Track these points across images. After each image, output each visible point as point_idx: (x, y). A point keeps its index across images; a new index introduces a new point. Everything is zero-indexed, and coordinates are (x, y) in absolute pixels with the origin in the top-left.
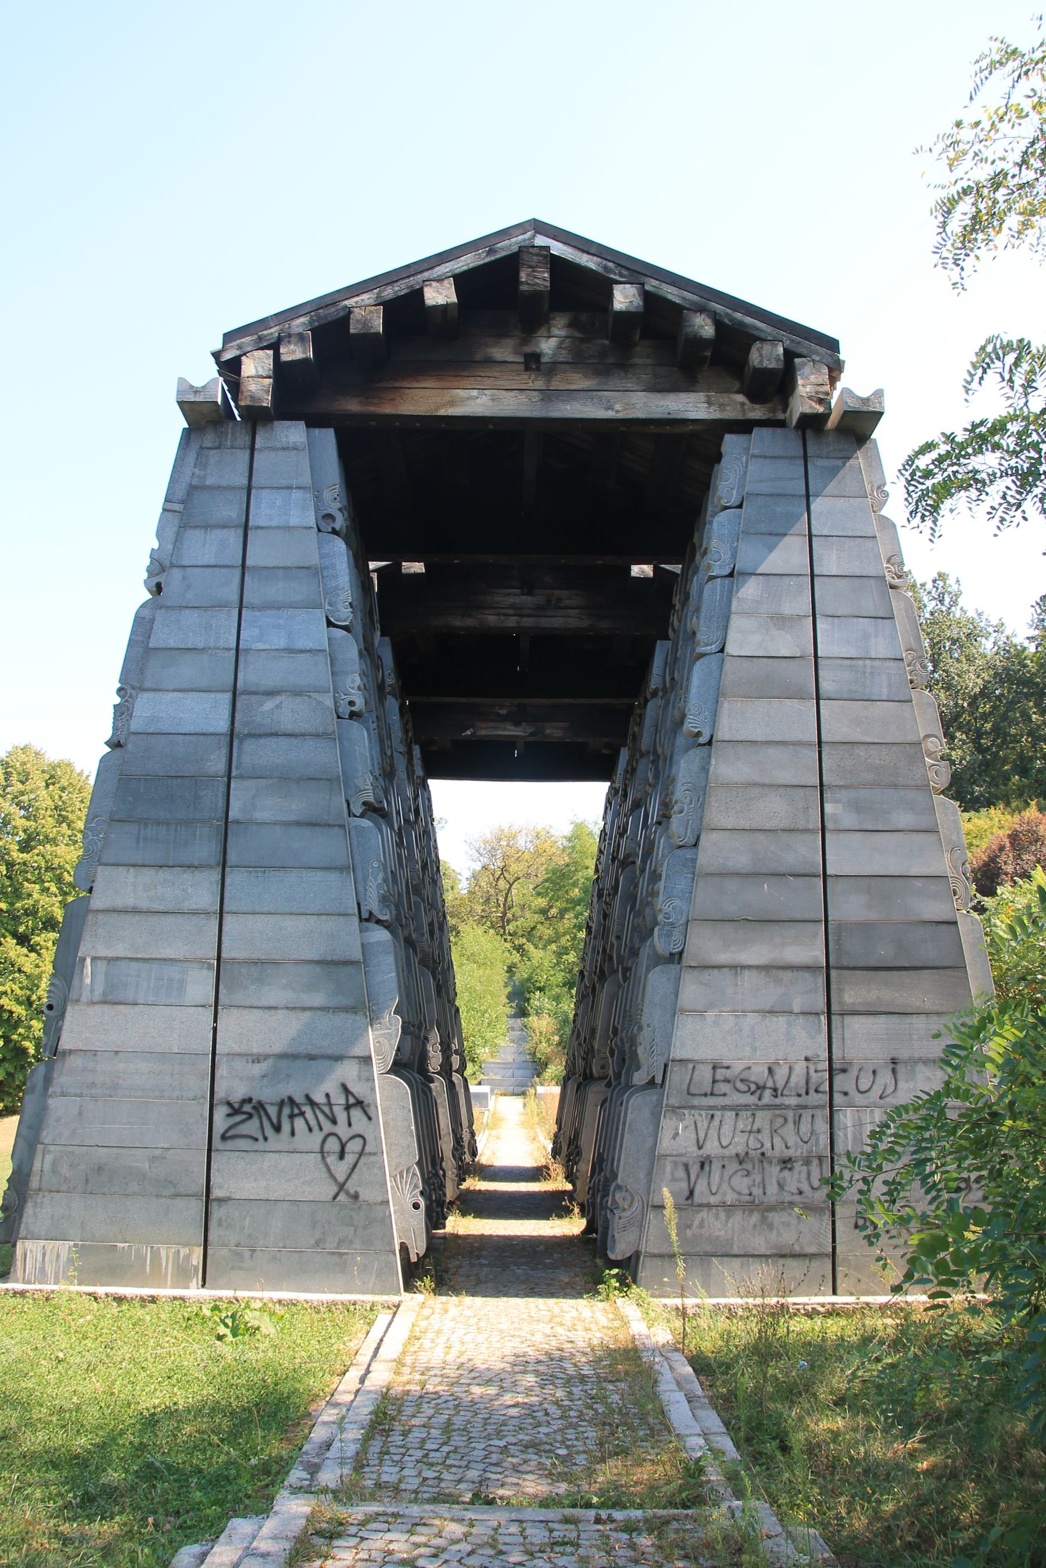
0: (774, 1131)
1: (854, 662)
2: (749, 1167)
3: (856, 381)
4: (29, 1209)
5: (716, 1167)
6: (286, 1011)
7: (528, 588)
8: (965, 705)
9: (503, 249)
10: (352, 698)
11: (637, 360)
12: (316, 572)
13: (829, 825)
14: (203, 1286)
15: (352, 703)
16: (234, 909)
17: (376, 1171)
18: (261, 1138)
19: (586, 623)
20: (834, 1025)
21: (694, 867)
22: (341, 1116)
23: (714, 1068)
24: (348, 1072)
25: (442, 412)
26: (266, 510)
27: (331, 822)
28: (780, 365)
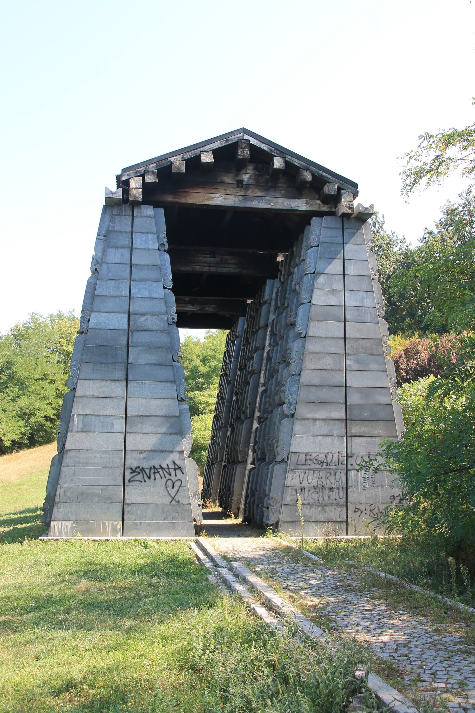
0: (327, 478)
1: (359, 308)
2: (318, 490)
3: (362, 201)
4: (55, 509)
5: (306, 490)
6: (152, 434)
7: (213, 255)
8: (384, 281)
9: (231, 140)
10: (173, 317)
11: (280, 185)
12: (159, 267)
13: (348, 368)
14: (123, 536)
15: (173, 319)
16: (131, 396)
17: (186, 492)
18: (143, 481)
19: (237, 271)
20: (348, 440)
21: (299, 383)
22: (173, 473)
23: (306, 455)
24: (175, 457)
25: (205, 203)
26: (140, 241)
27: (167, 364)
28: (336, 193)
